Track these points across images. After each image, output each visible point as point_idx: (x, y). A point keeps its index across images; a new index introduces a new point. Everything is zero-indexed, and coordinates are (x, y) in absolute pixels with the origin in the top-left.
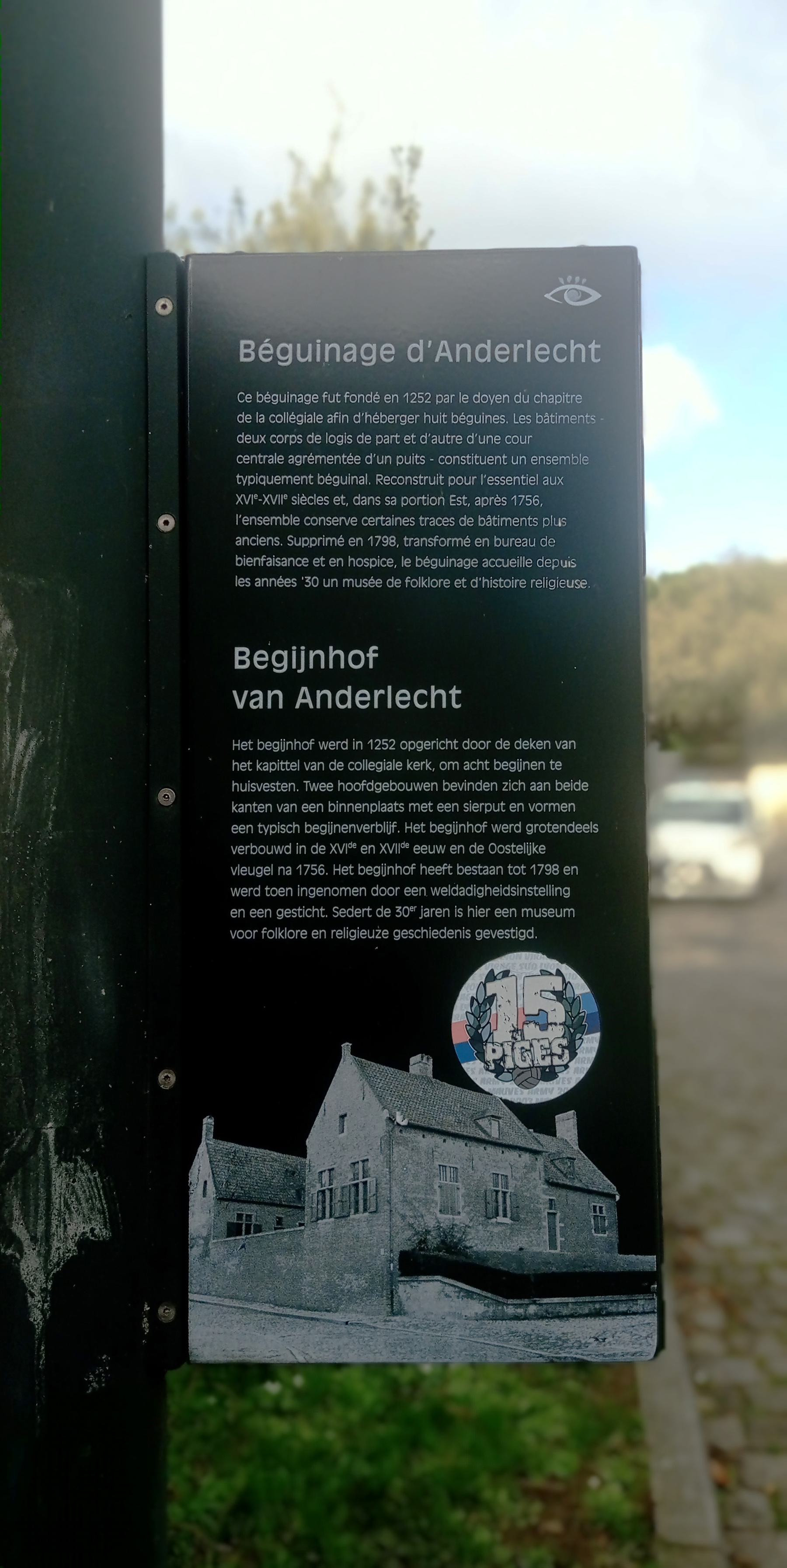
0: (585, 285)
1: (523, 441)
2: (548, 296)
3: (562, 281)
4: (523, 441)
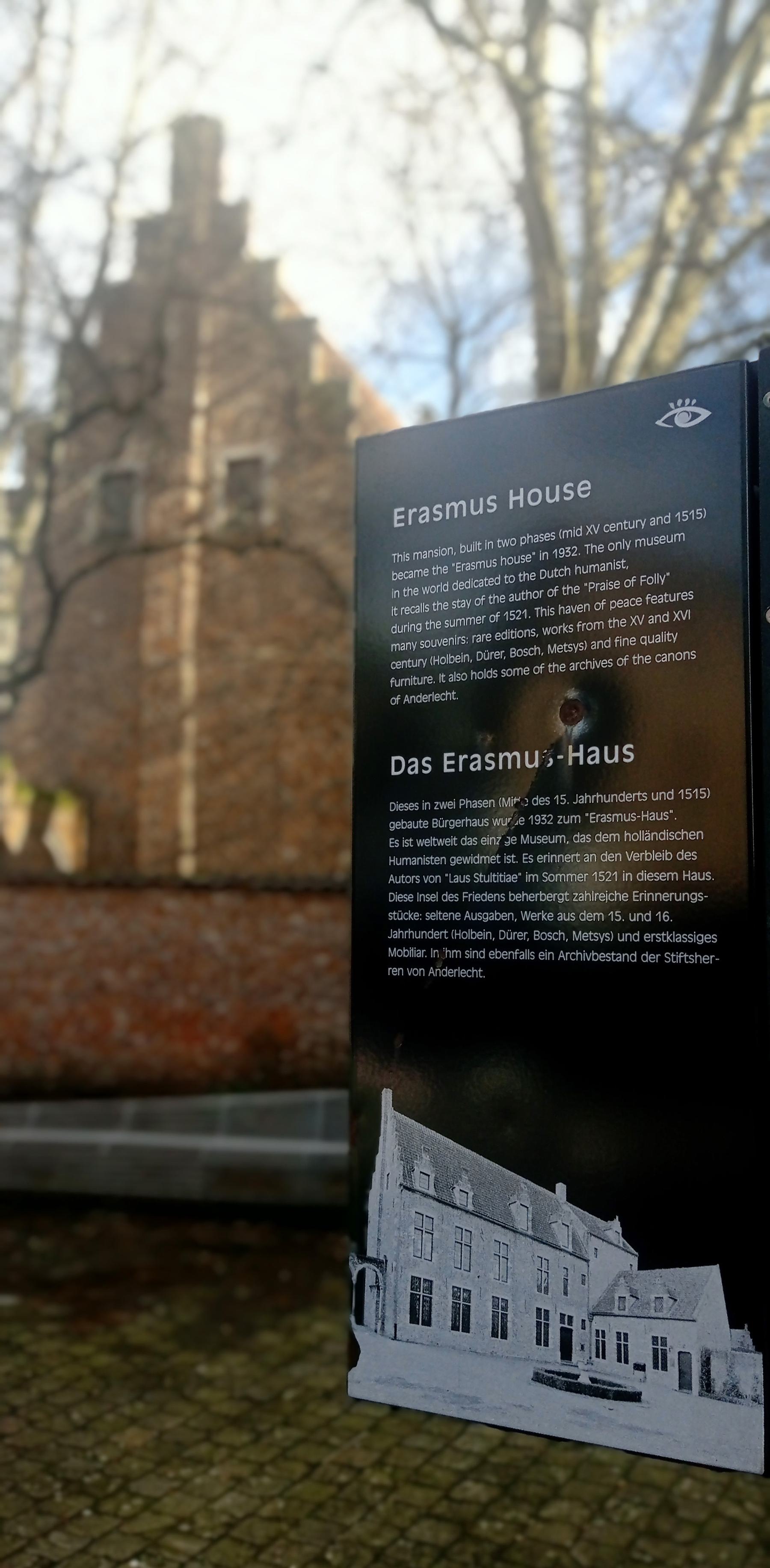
0: (695, 405)
1: (629, 936)
2: (659, 423)
3: (672, 405)
4: (629, 936)
